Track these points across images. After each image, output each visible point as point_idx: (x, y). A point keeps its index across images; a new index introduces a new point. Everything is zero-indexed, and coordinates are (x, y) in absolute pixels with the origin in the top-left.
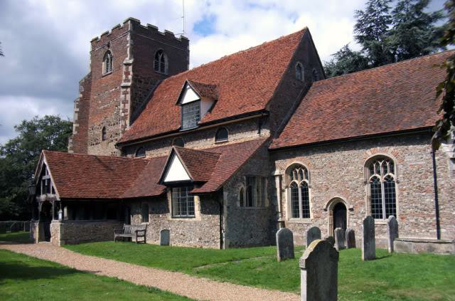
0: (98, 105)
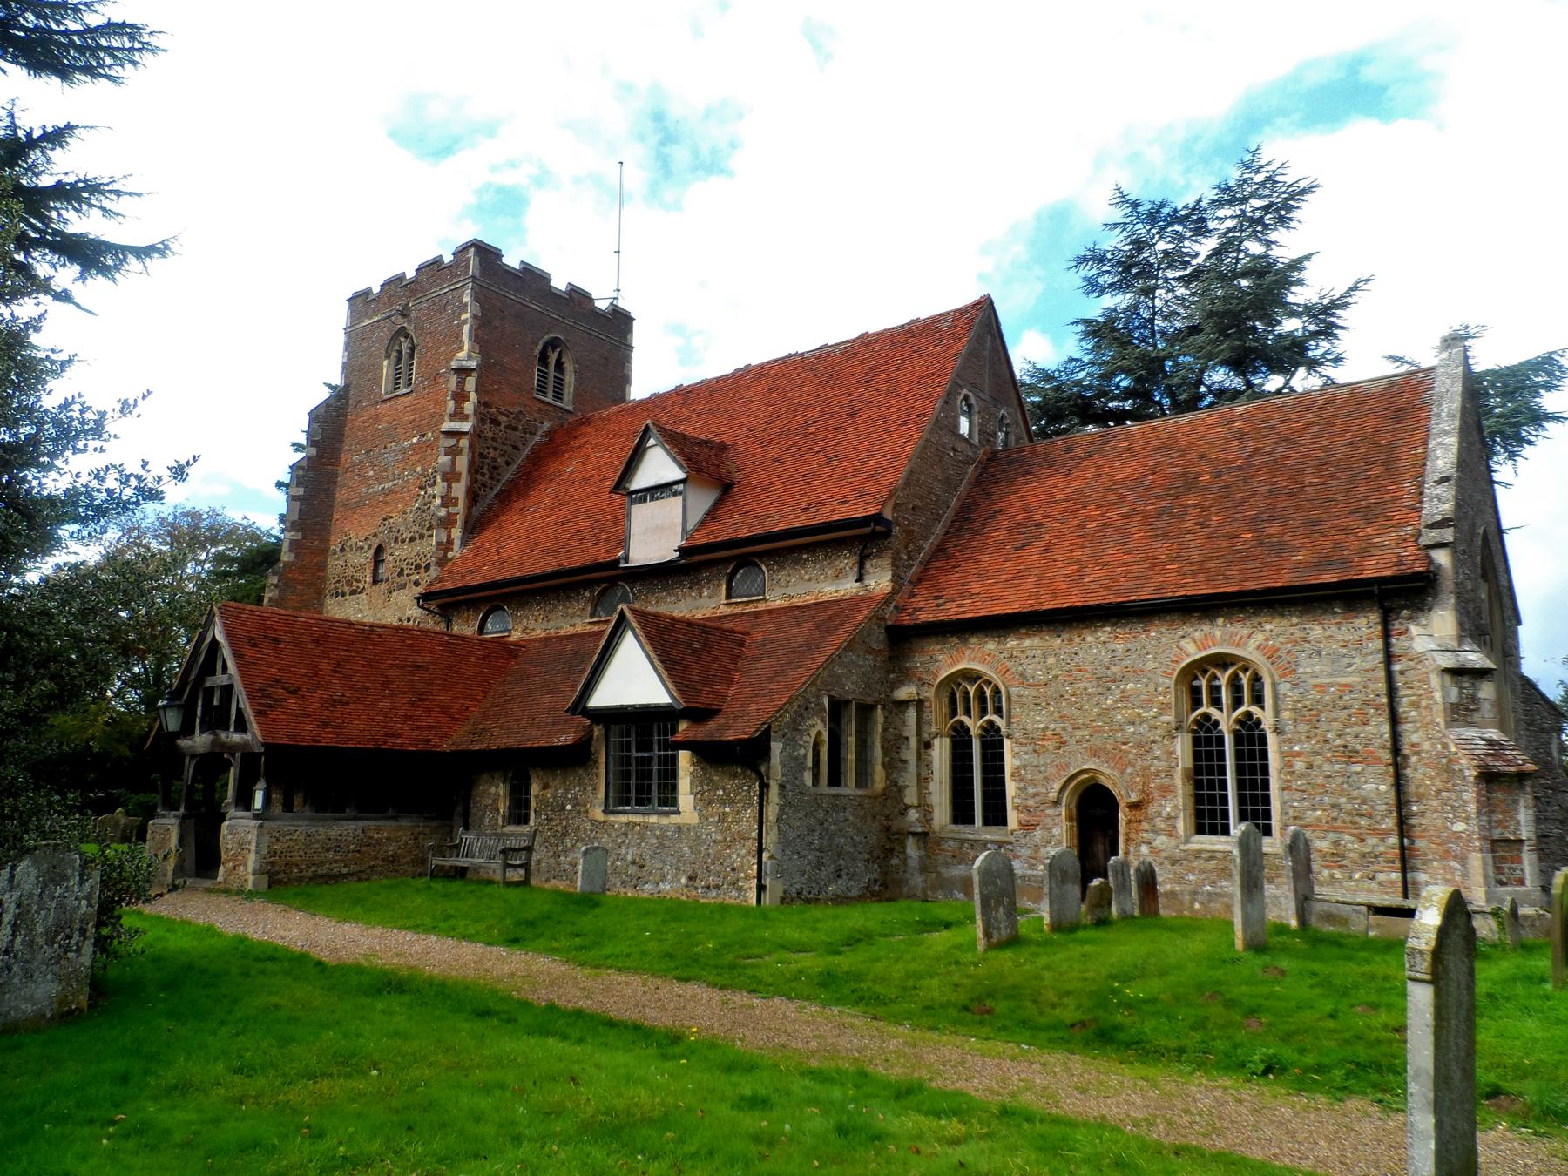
0: (364, 479)
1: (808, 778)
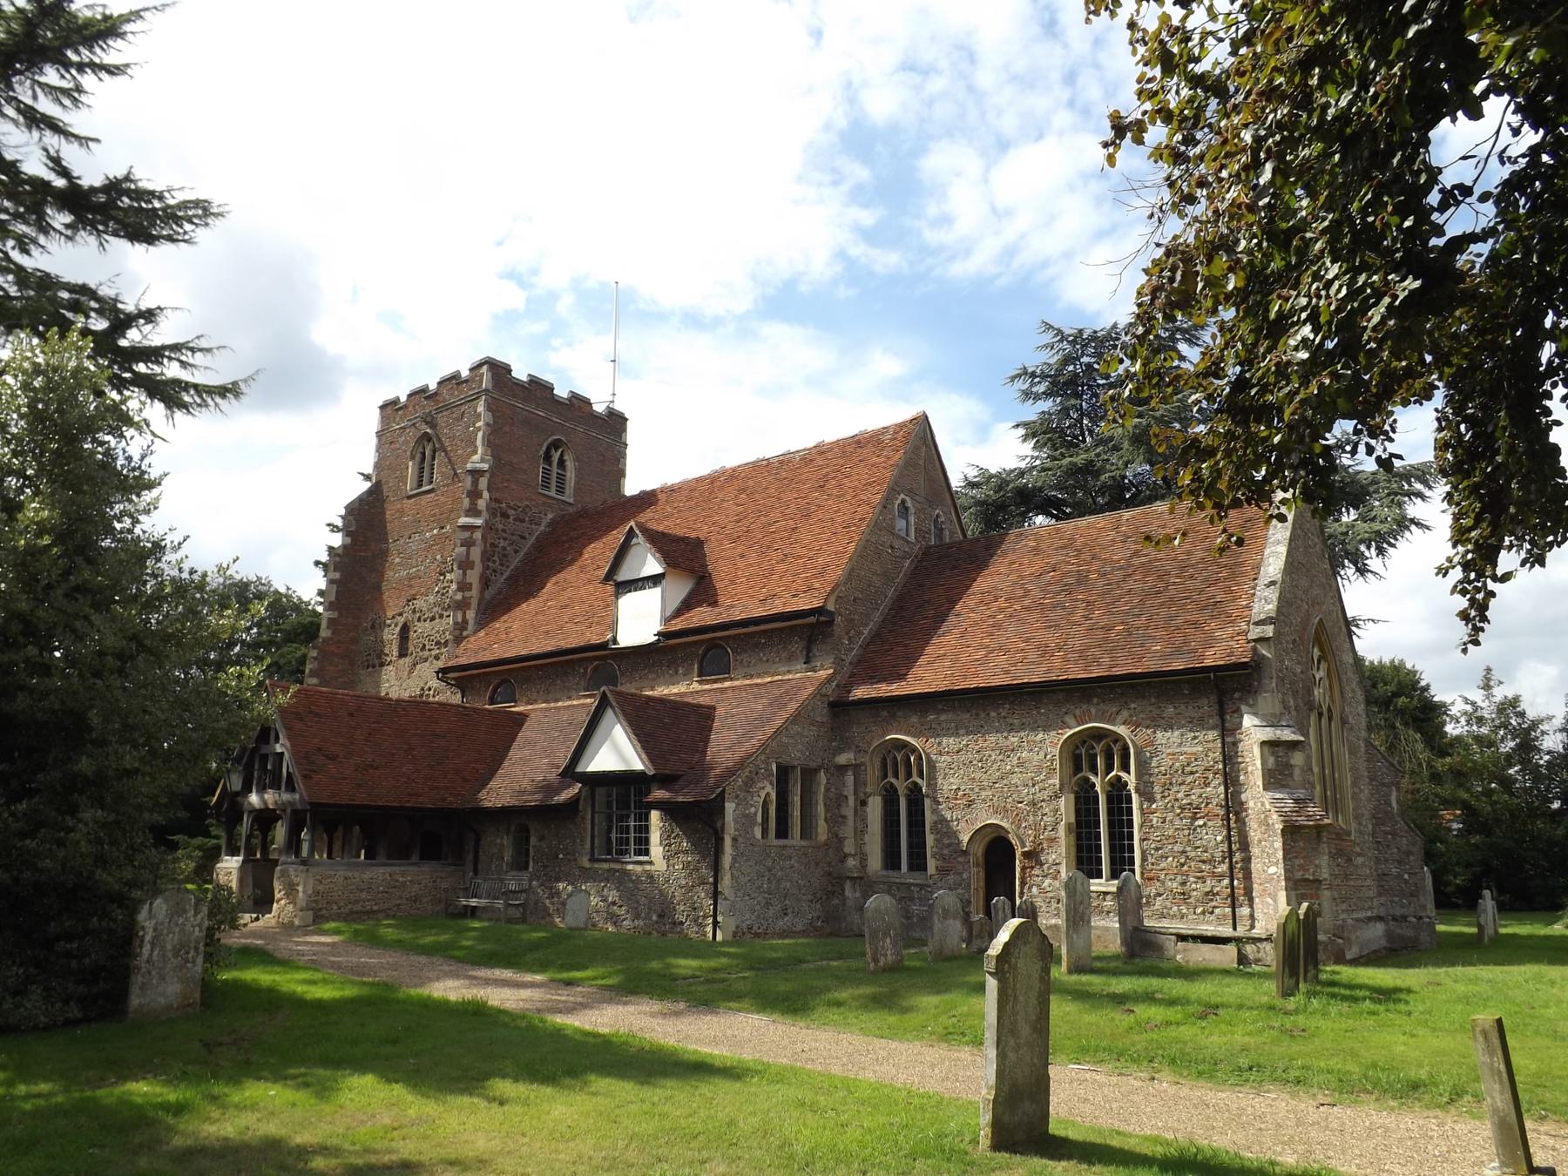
1: (758, 832)
